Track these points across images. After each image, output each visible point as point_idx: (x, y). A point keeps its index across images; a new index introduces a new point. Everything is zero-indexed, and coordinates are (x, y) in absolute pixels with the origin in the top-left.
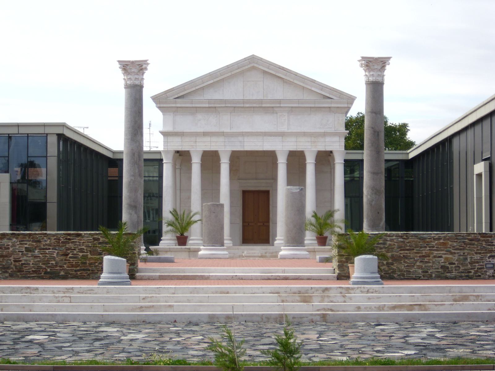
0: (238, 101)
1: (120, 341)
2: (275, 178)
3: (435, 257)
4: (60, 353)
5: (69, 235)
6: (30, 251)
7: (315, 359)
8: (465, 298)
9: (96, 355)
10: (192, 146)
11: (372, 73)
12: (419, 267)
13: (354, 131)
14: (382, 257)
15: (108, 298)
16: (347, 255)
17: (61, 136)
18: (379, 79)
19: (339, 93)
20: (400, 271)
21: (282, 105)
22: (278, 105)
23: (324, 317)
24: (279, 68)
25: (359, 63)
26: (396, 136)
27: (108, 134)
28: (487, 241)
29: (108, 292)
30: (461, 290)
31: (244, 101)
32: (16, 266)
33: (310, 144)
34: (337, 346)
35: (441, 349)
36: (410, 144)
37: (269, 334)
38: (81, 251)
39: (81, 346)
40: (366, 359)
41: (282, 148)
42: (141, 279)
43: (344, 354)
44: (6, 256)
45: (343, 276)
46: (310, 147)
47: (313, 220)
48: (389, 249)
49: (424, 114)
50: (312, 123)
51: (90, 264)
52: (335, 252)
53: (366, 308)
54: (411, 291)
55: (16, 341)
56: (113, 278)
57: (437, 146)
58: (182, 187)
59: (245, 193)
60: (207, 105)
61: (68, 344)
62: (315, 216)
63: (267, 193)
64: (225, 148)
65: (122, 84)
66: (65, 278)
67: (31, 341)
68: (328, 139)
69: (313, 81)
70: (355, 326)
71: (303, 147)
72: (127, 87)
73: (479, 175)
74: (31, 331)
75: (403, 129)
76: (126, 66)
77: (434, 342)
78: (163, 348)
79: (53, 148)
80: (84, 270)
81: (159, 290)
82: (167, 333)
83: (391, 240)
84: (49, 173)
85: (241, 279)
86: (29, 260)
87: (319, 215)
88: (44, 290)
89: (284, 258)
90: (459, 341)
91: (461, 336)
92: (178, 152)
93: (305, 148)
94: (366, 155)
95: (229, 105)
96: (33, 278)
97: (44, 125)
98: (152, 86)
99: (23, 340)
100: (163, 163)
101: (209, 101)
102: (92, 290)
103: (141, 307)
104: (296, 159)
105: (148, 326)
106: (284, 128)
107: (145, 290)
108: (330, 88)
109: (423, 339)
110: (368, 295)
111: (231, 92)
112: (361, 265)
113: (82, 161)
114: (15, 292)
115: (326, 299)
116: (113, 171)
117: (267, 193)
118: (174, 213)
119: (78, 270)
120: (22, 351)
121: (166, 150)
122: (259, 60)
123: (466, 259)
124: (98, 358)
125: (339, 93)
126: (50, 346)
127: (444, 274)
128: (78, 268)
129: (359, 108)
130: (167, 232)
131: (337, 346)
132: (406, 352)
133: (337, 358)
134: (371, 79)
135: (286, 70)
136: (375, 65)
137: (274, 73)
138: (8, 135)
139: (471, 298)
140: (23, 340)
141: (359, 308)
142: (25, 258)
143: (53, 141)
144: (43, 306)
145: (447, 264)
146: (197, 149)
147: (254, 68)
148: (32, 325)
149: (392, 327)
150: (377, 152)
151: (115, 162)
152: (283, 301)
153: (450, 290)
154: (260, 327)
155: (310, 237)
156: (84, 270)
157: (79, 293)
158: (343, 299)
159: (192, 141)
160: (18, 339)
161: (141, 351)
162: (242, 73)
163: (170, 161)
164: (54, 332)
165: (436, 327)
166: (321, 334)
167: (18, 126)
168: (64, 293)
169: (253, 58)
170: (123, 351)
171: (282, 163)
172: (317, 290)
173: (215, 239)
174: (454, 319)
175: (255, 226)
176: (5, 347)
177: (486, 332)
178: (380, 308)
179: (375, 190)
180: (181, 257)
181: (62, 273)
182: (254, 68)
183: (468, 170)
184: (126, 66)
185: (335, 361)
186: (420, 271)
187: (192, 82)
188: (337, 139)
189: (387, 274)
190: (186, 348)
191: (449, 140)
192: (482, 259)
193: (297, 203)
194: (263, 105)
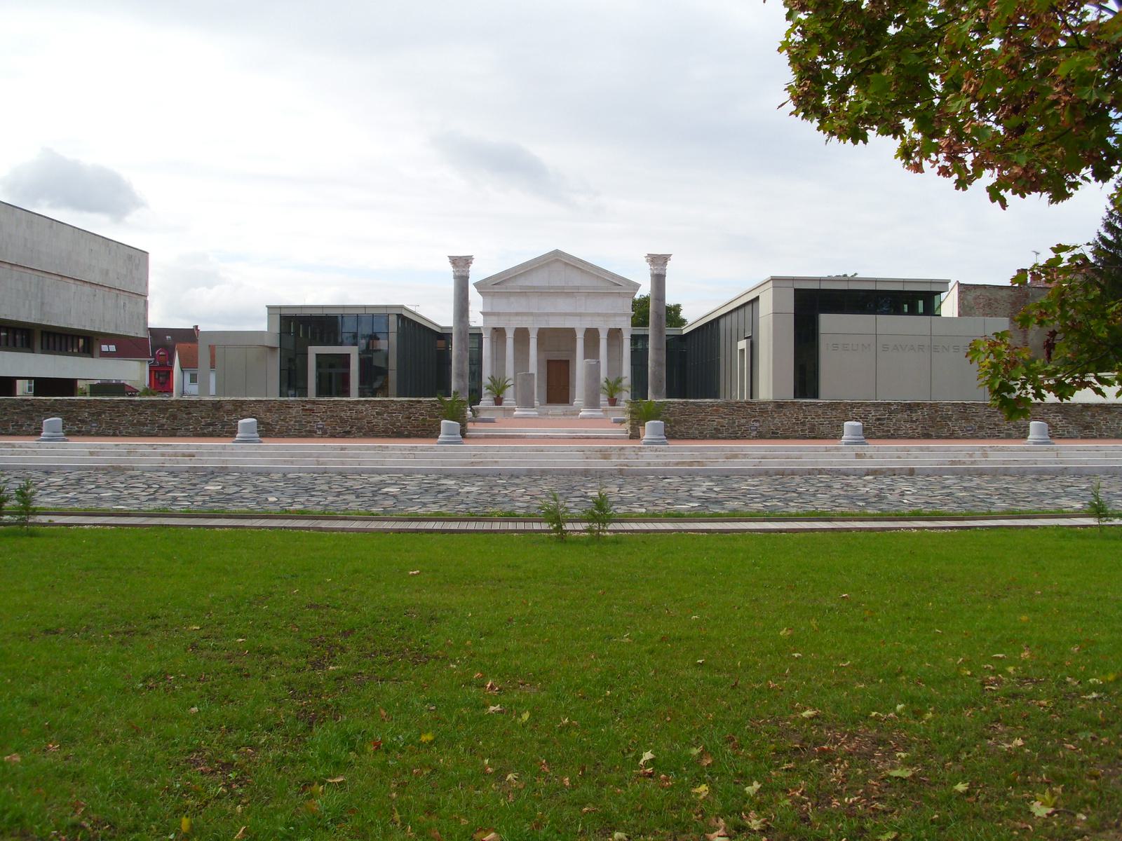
1: (458, 494)
2: (574, 350)
4: (411, 505)
5: (412, 401)
7: (619, 511)
8: (735, 456)
9: (441, 506)
12: (696, 429)
13: (641, 311)
14: (666, 421)
15: (444, 455)
16: (638, 419)
17: (400, 316)
18: (662, 272)
20: (681, 432)
23: (621, 472)
25: (645, 259)
26: (673, 315)
27: (440, 314)
28: (751, 408)
30: (731, 449)
31: (549, 288)
34: (635, 499)
35: (720, 502)
36: (683, 322)
37: (578, 488)
38: (422, 414)
39: (428, 498)
40: (660, 511)
41: (580, 326)
42: (471, 437)
43: (641, 506)
45: (635, 436)
47: (605, 385)
48: (672, 414)
49: (696, 301)
50: (605, 305)
52: (627, 417)
53: (655, 464)
54: (691, 450)
55: (374, 494)
56: (449, 438)
57: (706, 324)
58: (499, 356)
59: (549, 362)
61: (417, 496)
62: (607, 381)
63: (568, 362)
64: (533, 326)
65: (452, 274)
66: (408, 436)
67: (386, 494)
68: (618, 319)
70: (646, 480)
72: (455, 277)
73: (742, 351)
74: (384, 484)
75: (677, 309)
76: (455, 261)
77: (713, 495)
78: (494, 500)
79: (393, 327)
81: (486, 449)
82: (495, 486)
83: (674, 407)
84: (389, 344)
85: (552, 437)
86: (380, 422)
87: (610, 381)
88: (393, 449)
89: (583, 418)
90: (733, 494)
91: (734, 490)
92: (495, 328)
94: (650, 331)
97: (386, 307)
98: (477, 273)
99: (380, 492)
101: (521, 287)
102: (432, 448)
104: (592, 335)
105: (479, 479)
106: (582, 310)
107: (475, 448)
109: (703, 492)
110: (655, 452)
111: (523, 282)
112: (651, 429)
113: (414, 331)
115: (622, 457)
116: (441, 343)
117: (568, 362)
118: (492, 378)
120: (381, 502)
124: (444, 510)
126: (403, 498)
127: (716, 435)
129: (645, 290)
130: (485, 394)
131: (635, 499)
132: (692, 505)
133: (636, 510)
134: (655, 272)
136: (659, 262)
139: (740, 456)
140: (380, 492)
141: (649, 464)
142: (376, 420)
143: (393, 319)
144: (393, 461)
145: (719, 427)
146: (510, 326)
147: (557, 260)
148: (384, 477)
149: (676, 480)
150: (659, 331)
151: (443, 336)
152: (587, 458)
153: (723, 449)
154: (569, 480)
155: (603, 399)
157: (421, 450)
158: (636, 457)
160: (376, 491)
161: (476, 503)
162: (548, 264)
163: (489, 336)
164: (403, 484)
165: (712, 481)
166: (621, 487)
167: (365, 307)
168: (410, 450)
170: (462, 503)
172: (615, 448)
173: (527, 402)
174: (726, 474)
175: (557, 387)
176: (366, 499)
177: (754, 486)
178: (666, 464)
179: (658, 363)
180: (497, 415)
182: (557, 260)
183: (733, 346)
184: (455, 261)
185: (635, 512)
187: (506, 271)
188: (625, 318)
189: (671, 435)
190: (512, 500)
191: (717, 320)
192: (747, 422)
193: (593, 372)
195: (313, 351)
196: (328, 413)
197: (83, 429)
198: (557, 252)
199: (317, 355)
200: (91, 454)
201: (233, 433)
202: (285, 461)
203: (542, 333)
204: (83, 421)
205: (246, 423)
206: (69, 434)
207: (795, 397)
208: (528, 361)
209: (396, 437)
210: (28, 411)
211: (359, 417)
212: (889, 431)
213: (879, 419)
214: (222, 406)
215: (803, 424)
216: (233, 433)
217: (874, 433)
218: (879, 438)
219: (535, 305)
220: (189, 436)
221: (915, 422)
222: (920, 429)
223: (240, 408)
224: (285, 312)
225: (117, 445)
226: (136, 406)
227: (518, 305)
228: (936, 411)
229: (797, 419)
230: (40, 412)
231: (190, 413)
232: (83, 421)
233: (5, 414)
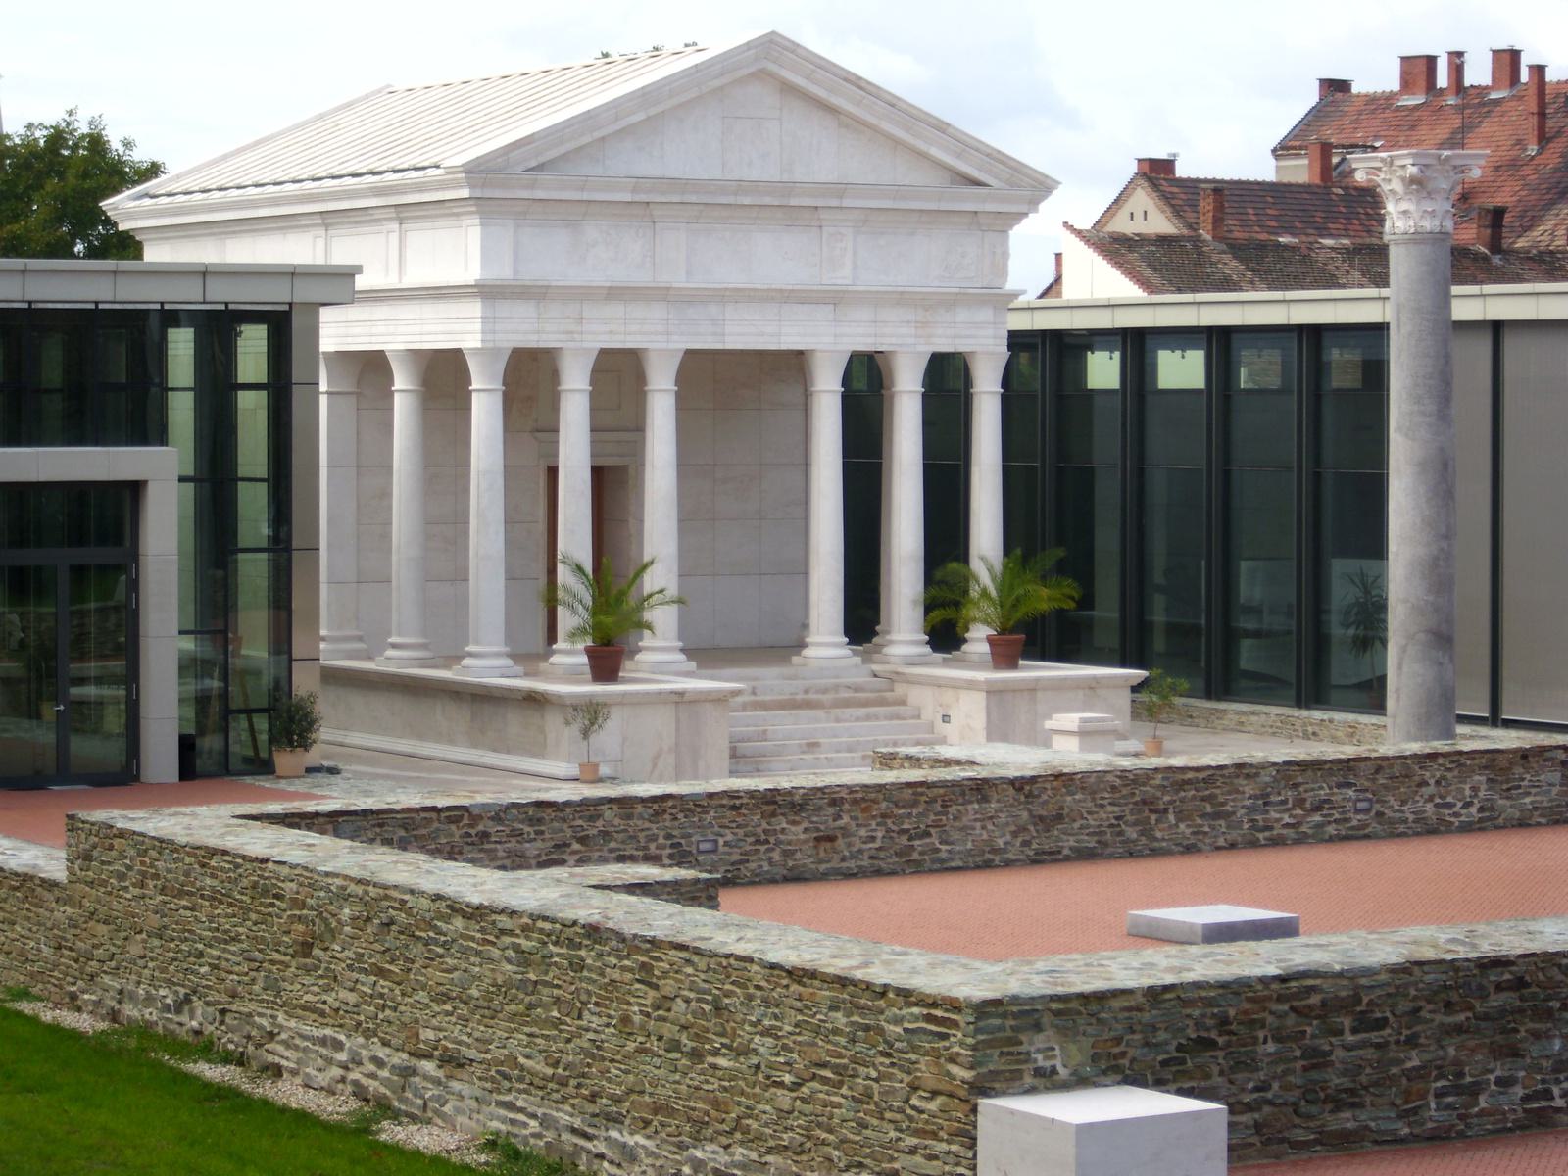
10: (568, 333)
19: (1011, 168)
21: (846, 203)
22: (834, 203)
24: (845, 80)
33: (913, 331)
46: (912, 341)
50: (921, 261)
60: (628, 197)
64: (664, 341)
68: (962, 315)
69: (941, 127)
71: (893, 340)
93: (900, 345)
95: (693, 199)
100: (470, 392)
101: (639, 182)
106: (842, 277)
108: (989, 151)
111: (688, 155)
121: (491, 345)
122: (786, 48)
125: (1011, 168)
135: (863, 85)
137: (822, 93)
138: (158, 306)
146: (577, 342)
147: (761, 75)
159: (569, 317)
169: (771, 42)
171: (911, 392)
182: (761, 75)
194: (793, 202)
198: (772, 45)
208: (1325, 287)
233: (1412, 1042)
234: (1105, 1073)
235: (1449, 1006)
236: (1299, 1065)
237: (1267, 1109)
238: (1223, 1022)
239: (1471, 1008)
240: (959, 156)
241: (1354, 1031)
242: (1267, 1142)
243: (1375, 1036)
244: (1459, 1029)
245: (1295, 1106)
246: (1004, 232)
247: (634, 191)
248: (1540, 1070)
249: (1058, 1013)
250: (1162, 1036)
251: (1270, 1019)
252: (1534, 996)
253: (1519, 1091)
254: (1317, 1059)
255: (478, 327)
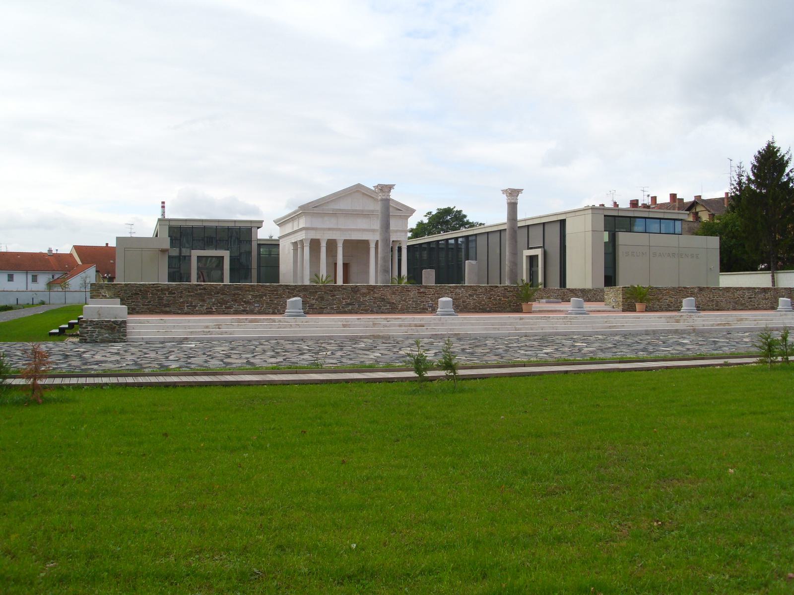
0: (348, 210)
3: (665, 299)
6: (471, 296)
8: (741, 320)
11: (384, 194)
22: (372, 213)
29: (584, 319)
32: (463, 305)
44: (458, 299)
51: (503, 304)
64: (340, 238)
66: (489, 312)
68: (399, 234)
80: (499, 307)
88: (553, 318)
96: (473, 312)
101: (333, 210)
103: (610, 326)
111: (344, 205)
114: (538, 319)
119: (497, 307)
123: (677, 300)
128: (497, 306)
147: (358, 191)
156: (499, 307)
181: (488, 309)
182: (358, 191)
186: (658, 307)
189: (699, 308)
195: (226, 254)
196: (436, 295)
197: (248, 309)
199: (198, 256)
200: (344, 326)
201: (434, 310)
202: (494, 328)
203: (347, 243)
204: (247, 302)
205: (688, 303)
206: (306, 313)
207: (343, 283)
209: (481, 312)
210: (201, 294)
211: (457, 297)
212: (754, 305)
213: (750, 298)
214: (358, 290)
215: (712, 301)
216: (434, 310)
217: (747, 307)
218: (750, 309)
219: (343, 223)
220: (333, 313)
221: (767, 299)
222: (769, 304)
223: (684, 292)
224: (172, 223)
225: (359, 319)
226: (293, 289)
227: (330, 223)
228: (777, 293)
229: (709, 298)
230: (211, 295)
231: (334, 296)
232: (247, 302)
233: (181, 297)
234: (116, 297)
235: (189, 292)
236: (157, 299)
237: (151, 306)
238: (140, 290)
239: (194, 292)
240: (396, 205)
241: (168, 294)
242: (150, 311)
243: (173, 295)
244: (191, 296)
245: (156, 306)
246: (407, 219)
247: (333, 211)
248: (210, 304)
249: (106, 286)
250: (128, 292)
251: (150, 291)
252: (208, 291)
253: (205, 307)
254: (161, 299)
255: (304, 235)
